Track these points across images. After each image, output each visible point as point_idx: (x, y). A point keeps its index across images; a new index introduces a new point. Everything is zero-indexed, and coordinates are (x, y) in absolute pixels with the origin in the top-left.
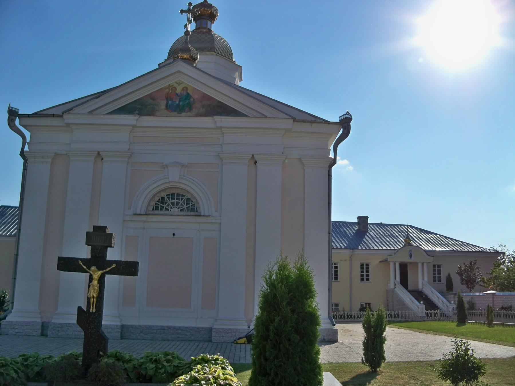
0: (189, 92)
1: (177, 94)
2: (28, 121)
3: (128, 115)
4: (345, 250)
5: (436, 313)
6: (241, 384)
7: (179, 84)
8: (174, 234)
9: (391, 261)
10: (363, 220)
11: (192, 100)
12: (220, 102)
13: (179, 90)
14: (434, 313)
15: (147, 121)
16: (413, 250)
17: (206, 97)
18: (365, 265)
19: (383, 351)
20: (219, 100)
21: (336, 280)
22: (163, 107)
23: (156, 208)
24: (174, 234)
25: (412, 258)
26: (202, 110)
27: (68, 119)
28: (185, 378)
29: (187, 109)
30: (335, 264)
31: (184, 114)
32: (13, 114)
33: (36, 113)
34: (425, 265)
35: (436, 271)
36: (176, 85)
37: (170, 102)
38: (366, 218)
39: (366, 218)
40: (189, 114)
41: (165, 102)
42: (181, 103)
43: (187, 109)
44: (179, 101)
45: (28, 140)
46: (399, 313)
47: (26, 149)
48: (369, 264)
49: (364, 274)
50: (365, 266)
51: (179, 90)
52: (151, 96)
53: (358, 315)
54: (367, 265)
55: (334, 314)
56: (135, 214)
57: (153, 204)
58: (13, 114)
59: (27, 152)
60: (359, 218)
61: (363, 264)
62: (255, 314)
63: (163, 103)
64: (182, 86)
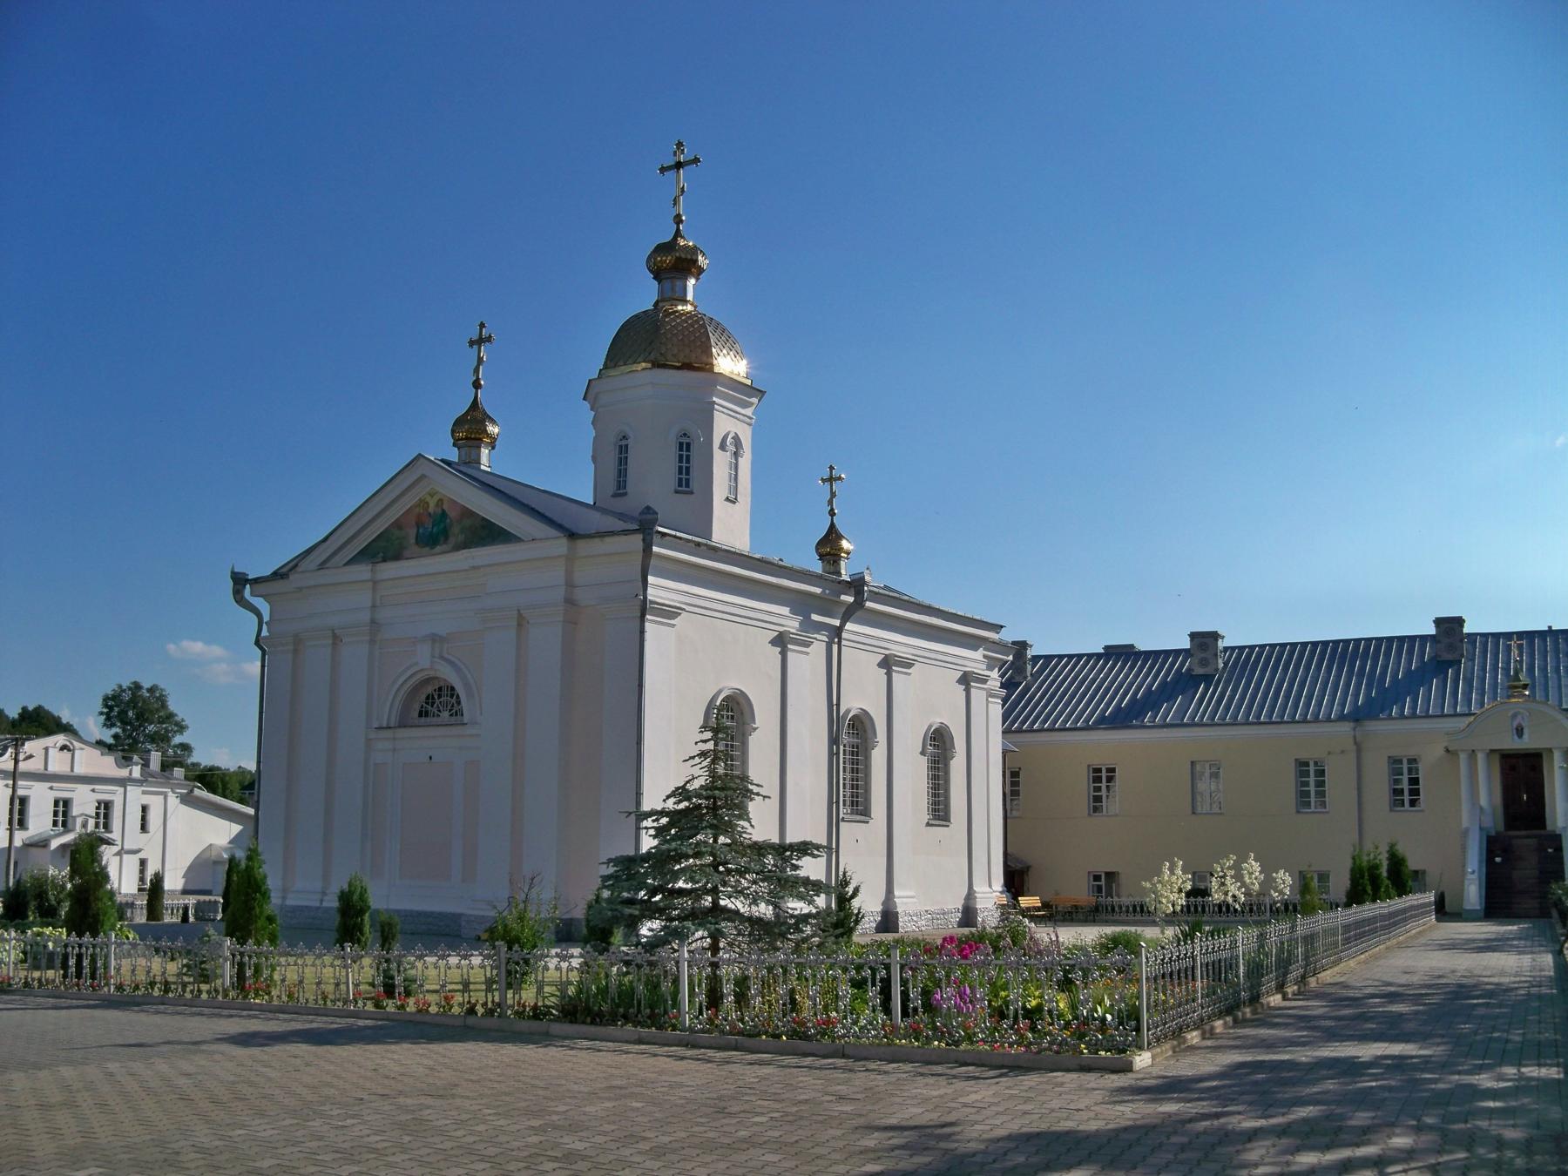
0: (445, 507)
1: (430, 514)
2: (261, 588)
4: (1338, 724)
6: (191, 919)
7: (432, 496)
8: (431, 758)
9: (1462, 750)
10: (1450, 626)
11: (448, 521)
12: (484, 519)
13: (432, 503)
15: (389, 570)
16: (1528, 714)
17: (467, 513)
20: (484, 516)
22: (413, 541)
23: (423, 713)
24: (431, 758)
25: (1526, 736)
26: (461, 538)
27: (295, 580)
28: (957, 1046)
29: (442, 539)
30: (1316, 763)
31: (438, 549)
32: (239, 580)
33: (275, 574)
34: (1480, 757)
35: (1101, 782)
36: (428, 499)
37: (421, 531)
38: (1459, 621)
39: (1459, 621)
40: (445, 547)
41: (415, 531)
43: (442, 539)
44: (433, 528)
45: (266, 618)
47: (265, 633)
48: (1418, 760)
49: (1101, 796)
50: (1104, 774)
51: (432, 503)
54: (1412, 761)
56: (380, 728)
57: (417, 707)
58: (239, 580)
59: (265, 637)
60: (1439, 622)
61: (1099, 770)
64: (436, 498)
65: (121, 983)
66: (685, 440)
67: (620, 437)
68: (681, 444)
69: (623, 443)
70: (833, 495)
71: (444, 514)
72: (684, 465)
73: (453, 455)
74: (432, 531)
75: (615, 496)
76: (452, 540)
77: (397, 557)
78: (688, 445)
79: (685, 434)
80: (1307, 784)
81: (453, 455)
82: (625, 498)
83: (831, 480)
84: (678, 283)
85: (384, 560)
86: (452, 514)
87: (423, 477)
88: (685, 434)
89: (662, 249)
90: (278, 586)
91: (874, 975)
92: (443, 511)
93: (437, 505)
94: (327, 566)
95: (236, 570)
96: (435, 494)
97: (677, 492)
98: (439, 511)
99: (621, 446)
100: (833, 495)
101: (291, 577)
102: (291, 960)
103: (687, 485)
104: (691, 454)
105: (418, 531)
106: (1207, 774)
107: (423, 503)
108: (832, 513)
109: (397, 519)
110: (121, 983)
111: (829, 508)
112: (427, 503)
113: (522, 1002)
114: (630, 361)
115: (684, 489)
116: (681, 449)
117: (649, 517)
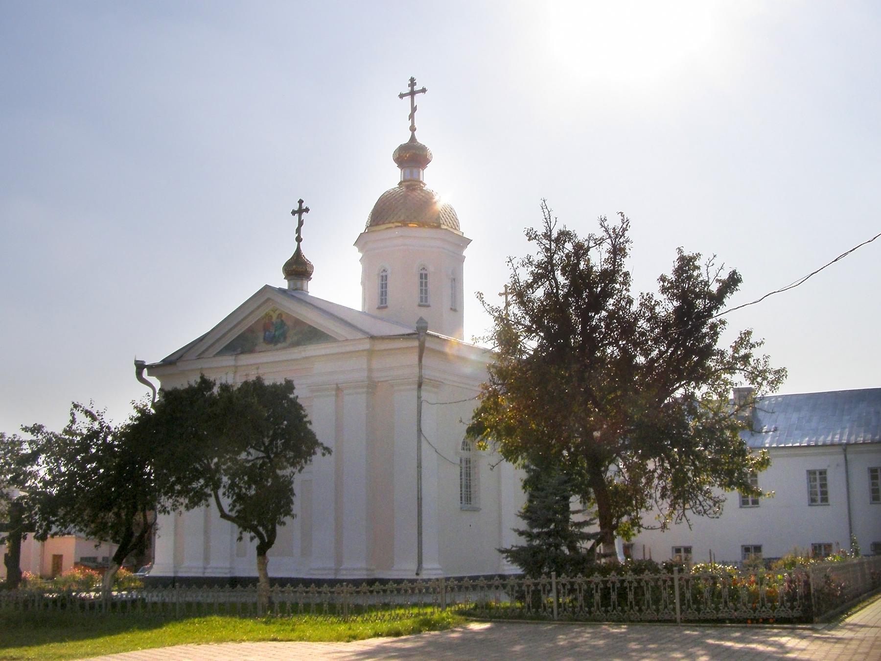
0: (283, 318)
3: (154, 551)
5: (660, 583)
11: (286, 327)
14: (635, 584)
18: (818, 473)
19: (11, 541)
21: (877, 500)
22: (262, 340)
27: (181, 366)
31: (279, 345)
32: (140, 366)
36: (272, 313)
42: (277, 333)
44: (275, 332)
46: (626, 584)
52: (250, 330)
53: (658, 587)
55: (536, 585)
58: (140, 366)
62: (219, 568)
63: (261, 335)
65: (663, 500)
66: (424, 272)
67: (382, 270)
68: (421, 275)
69: (384, 274)
70: (414, 109)
71: (283, 323)
72: (424, 288)
73: (284, 284)
74: (275, 334)
75: (379, 308)
76: (289, 341)
77: (251, 351)
78: (426, 275)
79: (424, 269)
80: (815, 486)
81: (284, 284)
82: (386, 310)
83: (300, 211)
84: (415, 170)
85: (242, 353)
86: (289, 323)
87: (268, 299)
88: (424, 269)
89: (403, 149)
90: (169, 370)
91: (597, 587)
92: (282, 321)
93: (278, 318)
94: (202, 357)
95: (137, 359)
96: (276, 310)
97: (420, 306)
98: (279, 320)
99: (382, 276)
100: (414, 109)
101: (178, 364)
102: (234, 594)
103: (426, 301)
104: (428, 280)
105: (265, 333)
106: (749, 476)
107: (268, 316)
108: (299, 240)
109: (251, 326)
110: (663, 500)
111: (297, 235)
112: (271, 316)
113: (514, 569)
114: (381, 222)
115: (423, 303)
116: (421, 278)
117: (424, 325)
